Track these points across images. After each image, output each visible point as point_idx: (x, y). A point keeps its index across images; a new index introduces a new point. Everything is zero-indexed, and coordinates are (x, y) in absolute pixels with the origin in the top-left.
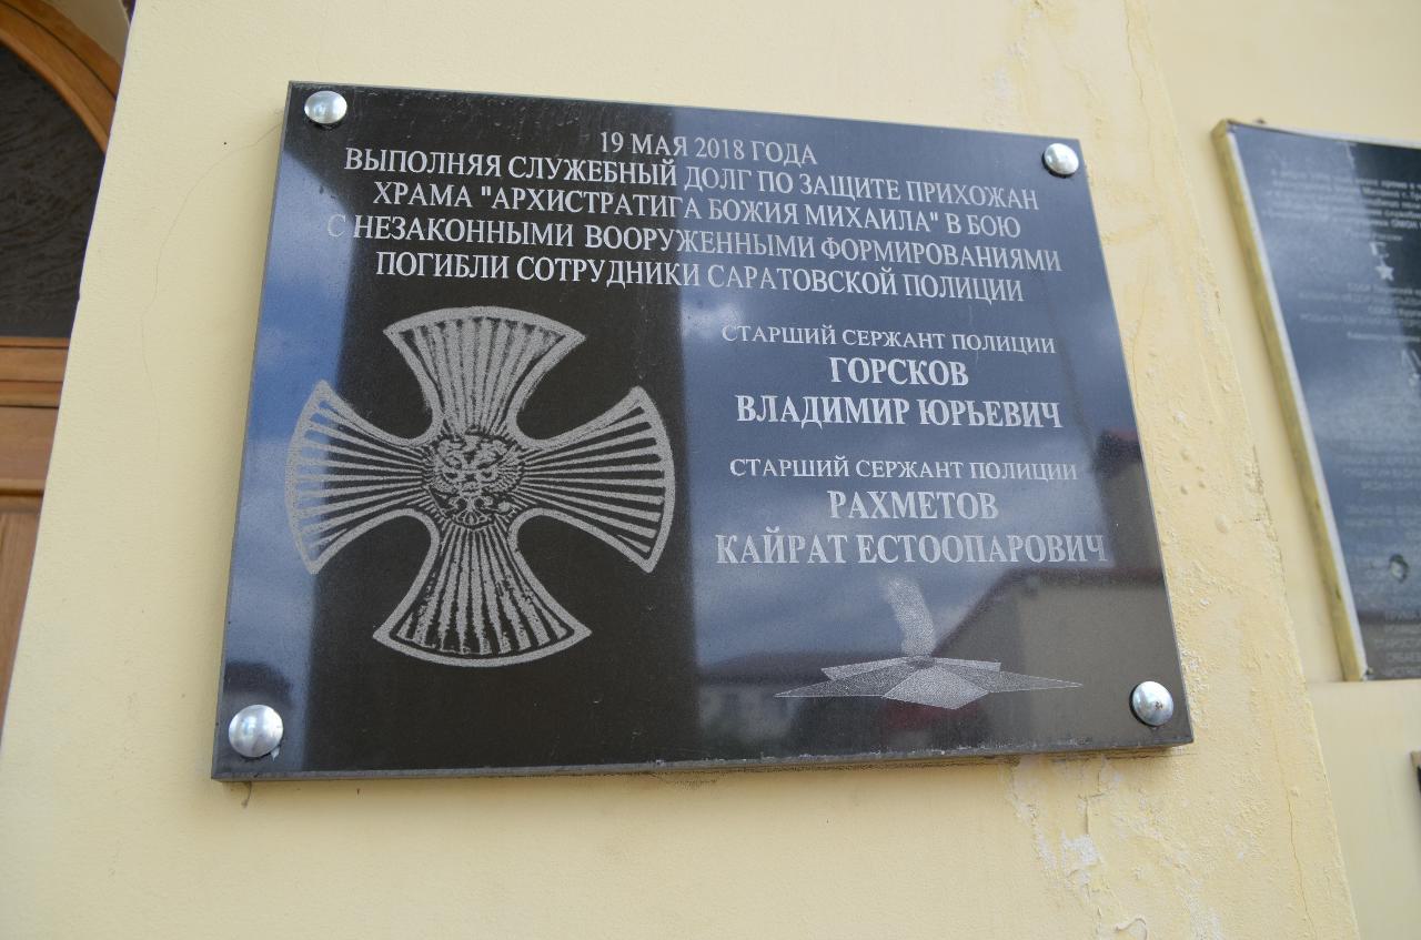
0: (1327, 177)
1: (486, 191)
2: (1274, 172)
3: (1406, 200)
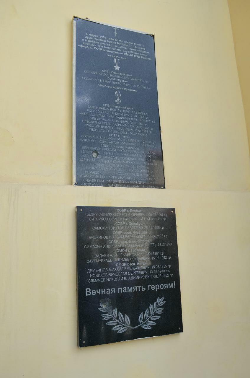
0: (106, 38)
1: (118, 43)
2: (87, 34)
3: (131, 48)
